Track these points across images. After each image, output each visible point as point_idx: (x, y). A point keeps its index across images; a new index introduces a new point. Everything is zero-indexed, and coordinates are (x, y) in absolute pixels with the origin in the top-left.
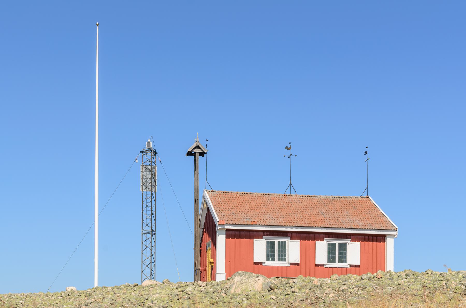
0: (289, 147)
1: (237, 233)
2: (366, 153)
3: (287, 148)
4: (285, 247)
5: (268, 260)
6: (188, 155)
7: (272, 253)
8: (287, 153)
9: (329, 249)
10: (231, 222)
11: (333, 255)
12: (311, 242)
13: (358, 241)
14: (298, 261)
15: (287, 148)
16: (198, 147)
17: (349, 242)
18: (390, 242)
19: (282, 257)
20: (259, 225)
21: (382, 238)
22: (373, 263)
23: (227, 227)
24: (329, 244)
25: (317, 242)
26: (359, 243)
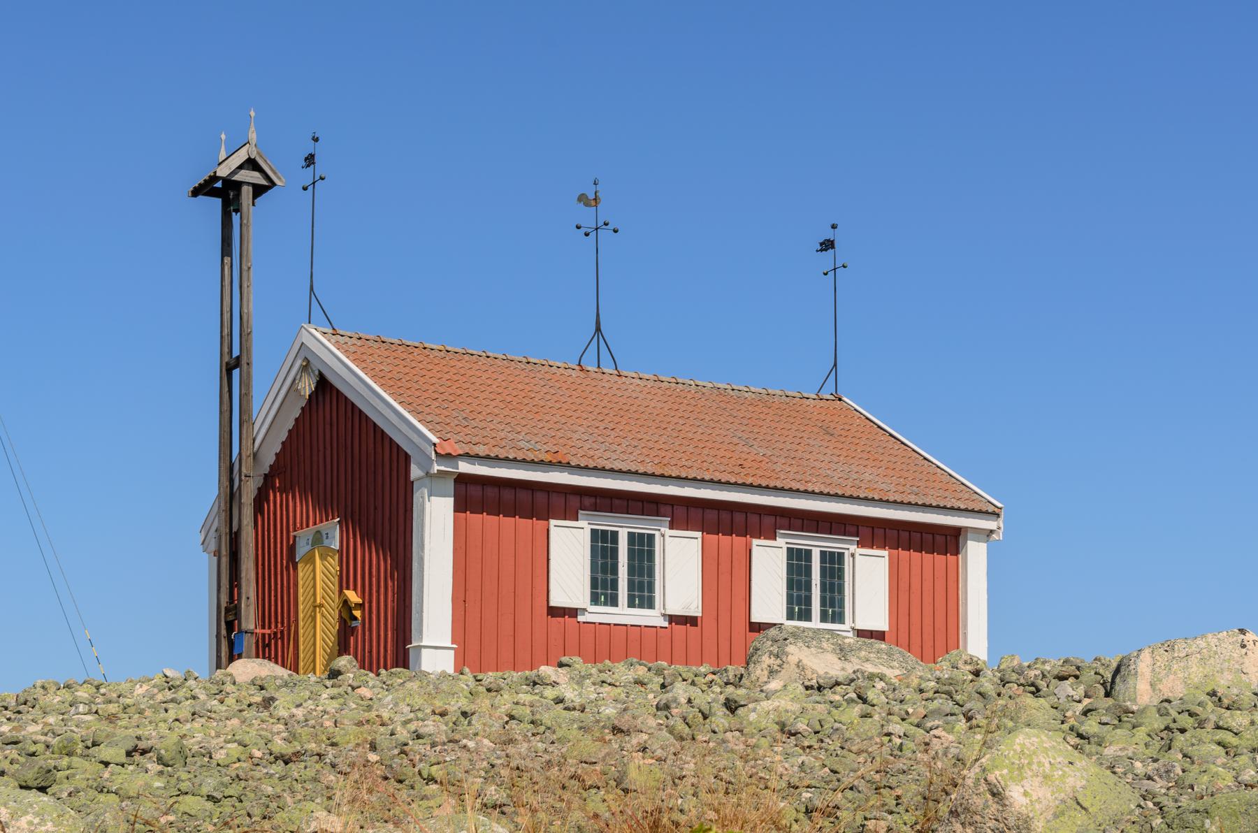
0: (592, 196)
1: (491, 492)
2: (310, 160)
3: (582, 198)
4: (651, 555)
5: (595, 600)
6: (196, 192)
7: (609, 577)
8: (587, 217)
9: (790, 568)
10: (481, 450)
11: (803, 593)
12: (738, 541)
13: (884, 548)
14: (695, 609)
15: (582, 198)
16: (251, 164)
17: (853, 548)
18: (976, 554)
19: (642, 594)
20: (578, 467)
21: (948, 542)
22: (925, 623)
23: (465, 467)
24: (790, 551)
25: (755, 542)
26: (885, 553)
